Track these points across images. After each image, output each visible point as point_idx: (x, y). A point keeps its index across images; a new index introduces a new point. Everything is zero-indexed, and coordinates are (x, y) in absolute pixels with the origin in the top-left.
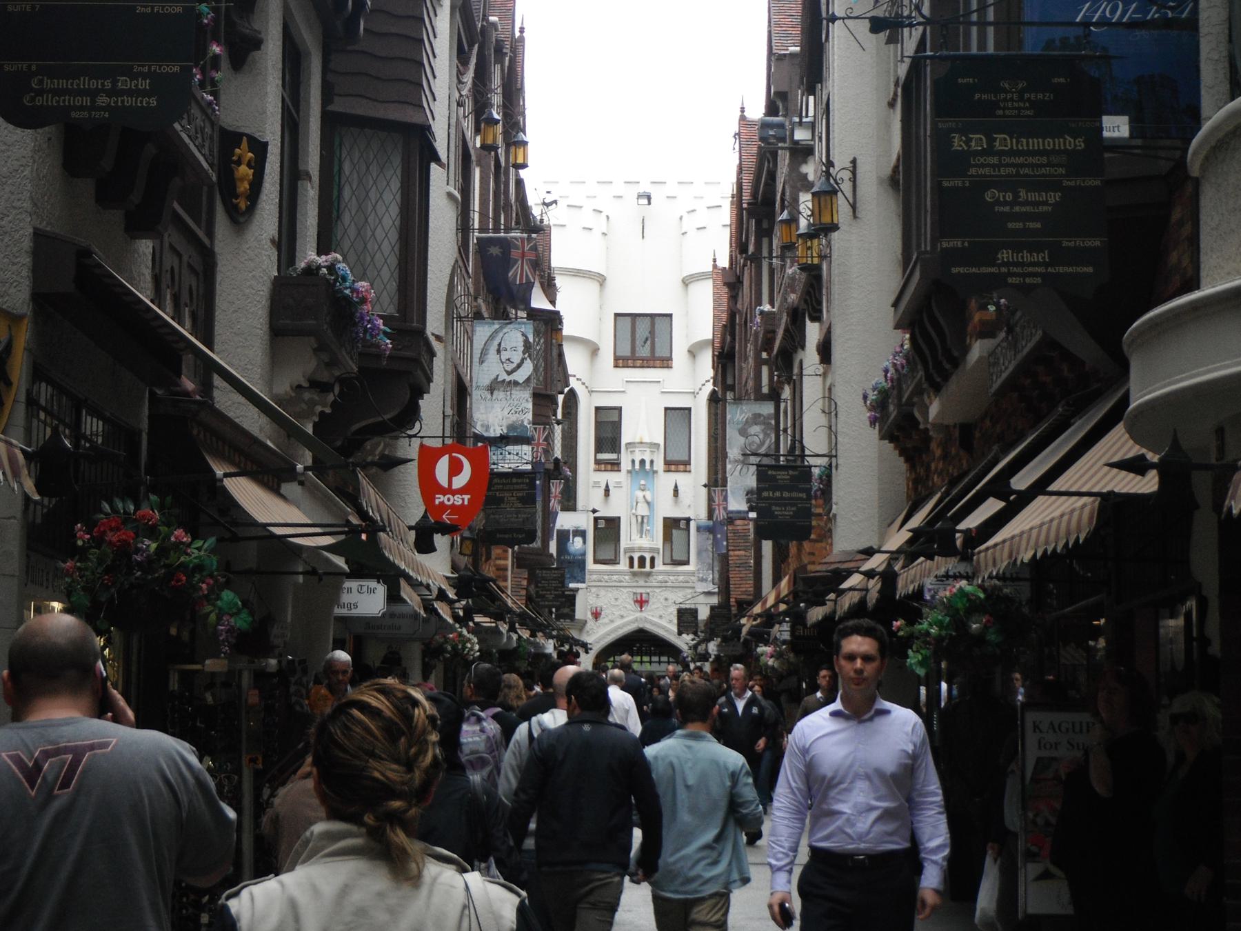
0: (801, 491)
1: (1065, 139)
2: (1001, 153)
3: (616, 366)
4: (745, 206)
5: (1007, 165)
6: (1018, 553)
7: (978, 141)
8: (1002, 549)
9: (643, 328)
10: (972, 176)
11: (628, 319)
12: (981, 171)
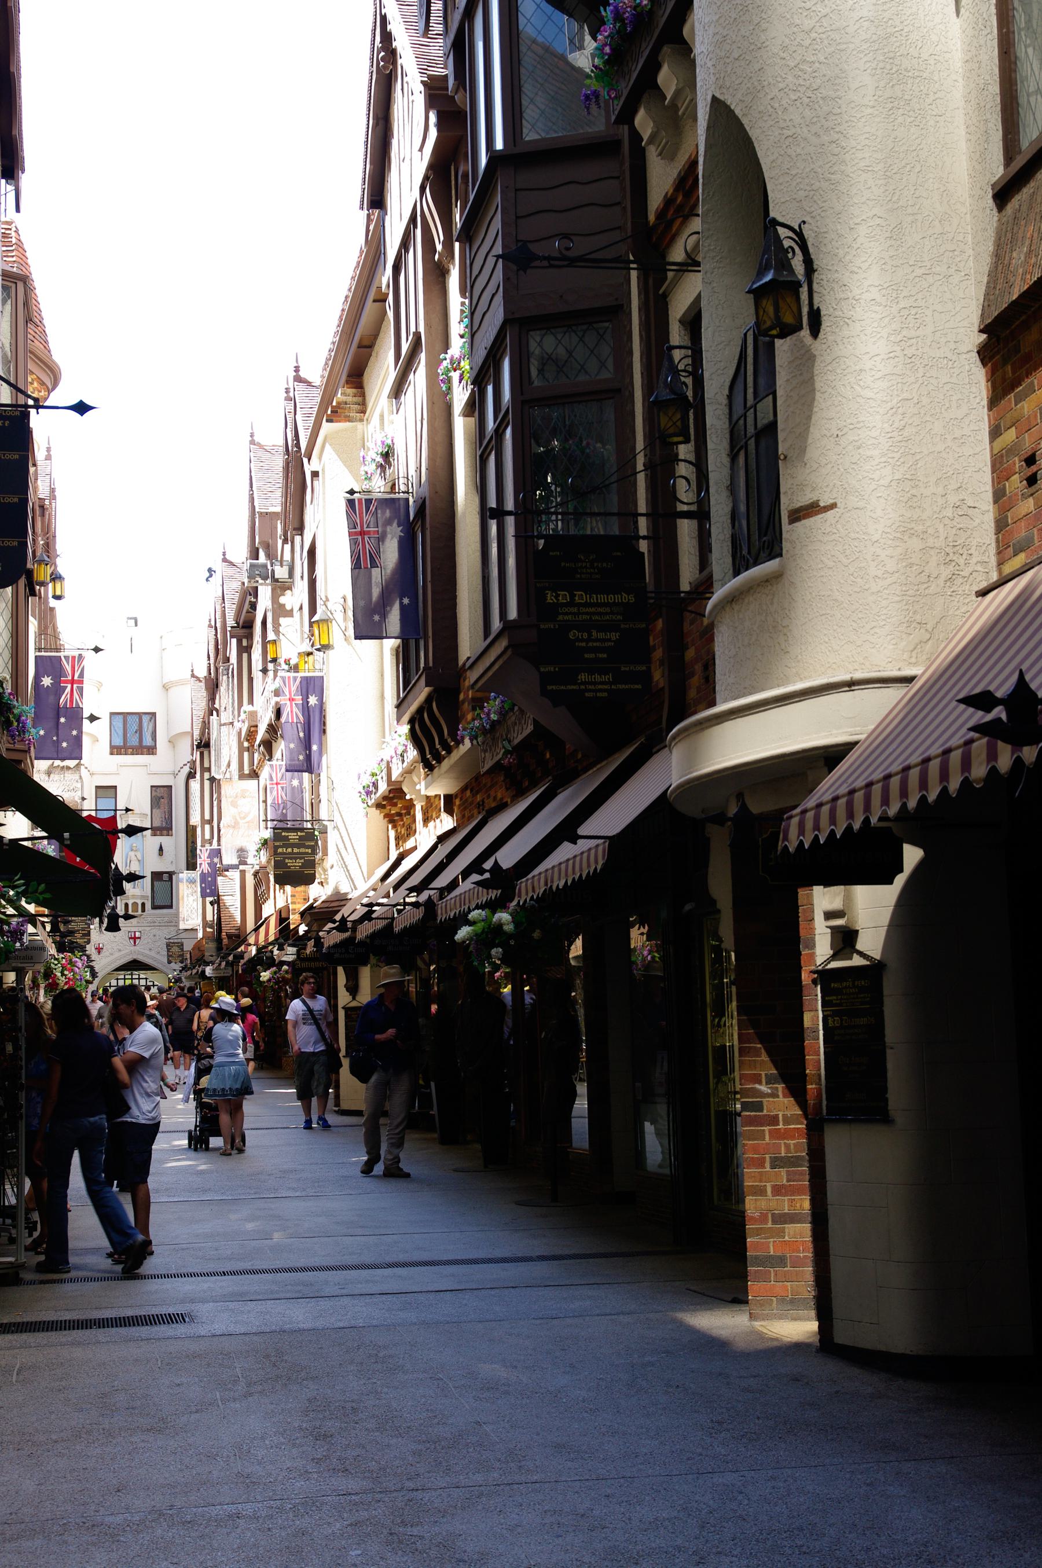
0: (308, 847)
1: (622, 596)
2: (580, 605)
3: (112, 754)
4: (229, 629)
5: (583, 613)
6: (552, 882)
7: (564, 597)
8: (539, 880)
9: (133, 726)
10: (560, 621)
11: (121, 717)
12: (566, 618)
